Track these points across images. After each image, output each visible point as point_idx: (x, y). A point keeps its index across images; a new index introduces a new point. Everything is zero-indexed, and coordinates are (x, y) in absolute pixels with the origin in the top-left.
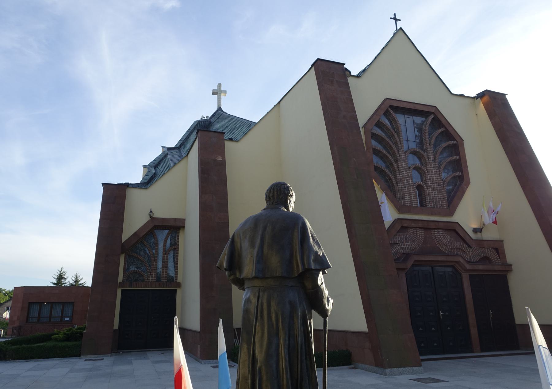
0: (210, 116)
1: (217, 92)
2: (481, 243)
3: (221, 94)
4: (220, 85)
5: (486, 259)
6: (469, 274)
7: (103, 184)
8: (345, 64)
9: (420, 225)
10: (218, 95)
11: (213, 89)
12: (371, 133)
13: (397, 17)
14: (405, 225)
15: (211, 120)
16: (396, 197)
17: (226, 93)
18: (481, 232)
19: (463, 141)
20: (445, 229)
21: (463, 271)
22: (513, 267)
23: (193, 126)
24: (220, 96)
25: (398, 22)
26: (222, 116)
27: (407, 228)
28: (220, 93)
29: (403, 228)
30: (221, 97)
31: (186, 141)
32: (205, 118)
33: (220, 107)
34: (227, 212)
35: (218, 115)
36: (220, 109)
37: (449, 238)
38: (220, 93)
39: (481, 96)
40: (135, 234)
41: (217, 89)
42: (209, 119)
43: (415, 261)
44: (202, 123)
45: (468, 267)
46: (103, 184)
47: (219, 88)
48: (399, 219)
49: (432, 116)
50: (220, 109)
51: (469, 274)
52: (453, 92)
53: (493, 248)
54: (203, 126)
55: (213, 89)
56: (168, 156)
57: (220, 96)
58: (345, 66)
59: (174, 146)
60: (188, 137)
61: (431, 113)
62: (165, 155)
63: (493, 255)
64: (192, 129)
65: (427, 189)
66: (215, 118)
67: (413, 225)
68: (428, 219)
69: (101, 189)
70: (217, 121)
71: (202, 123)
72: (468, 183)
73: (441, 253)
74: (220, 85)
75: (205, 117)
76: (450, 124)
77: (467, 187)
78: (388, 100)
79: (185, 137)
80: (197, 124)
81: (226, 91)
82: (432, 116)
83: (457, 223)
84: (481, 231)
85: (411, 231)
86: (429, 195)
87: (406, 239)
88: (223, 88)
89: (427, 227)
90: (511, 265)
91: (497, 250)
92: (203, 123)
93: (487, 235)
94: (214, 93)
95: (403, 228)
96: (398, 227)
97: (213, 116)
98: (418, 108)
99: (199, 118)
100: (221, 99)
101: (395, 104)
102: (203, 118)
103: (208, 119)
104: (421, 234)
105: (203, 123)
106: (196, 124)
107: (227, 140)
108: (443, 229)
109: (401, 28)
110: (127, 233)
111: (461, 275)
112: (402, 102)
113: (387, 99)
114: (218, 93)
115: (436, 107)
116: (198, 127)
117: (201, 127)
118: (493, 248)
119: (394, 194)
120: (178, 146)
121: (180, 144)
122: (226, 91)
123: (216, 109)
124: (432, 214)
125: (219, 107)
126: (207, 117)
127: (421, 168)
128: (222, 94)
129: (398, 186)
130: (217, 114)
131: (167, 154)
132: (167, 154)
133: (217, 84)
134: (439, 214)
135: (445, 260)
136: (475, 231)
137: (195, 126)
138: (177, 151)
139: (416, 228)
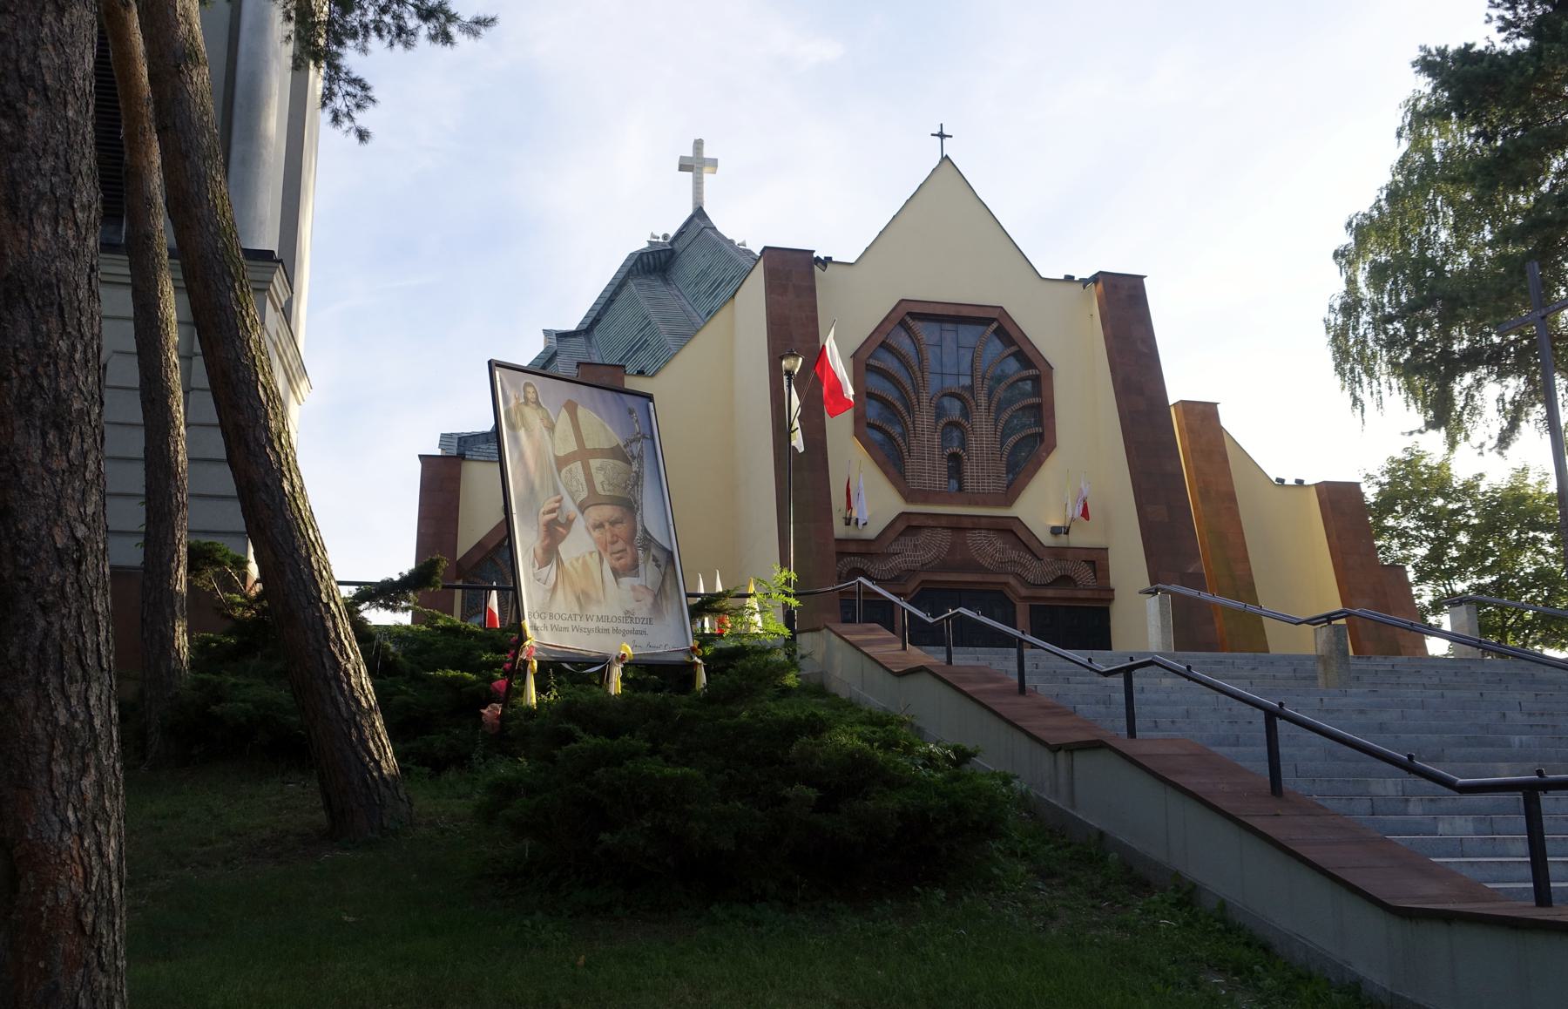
0: (672, 234)
1: (695, 164)
2: (1059, 553)
3: (701, 169)
4: (698, 144)
5: (1065, 580)
6: (1030, 605)
7: (420, 456)
8: (814, 251)
9: (944, 522)
10: (695, 171)
11: (681, 157)
12: (867, 365)
13: (945, 132)
14: (914, 523)
15: (676, 246)
16: (905, 479)
17: (716, 166)
18: (1067, 533)
19: (1052, 369)
20: (994, 530)
21: (1018, 600)
22: (1116, 593)
23: (625, 270)
24: (698, 176)
25: (946, 141)
26: (700, 238)
27: (919, 528)
28: (699, 166)
29: (909, 528)
30: (702, 178)
31: (605, 312)
32: (661, 240)
33: (701, 209)
34: (1230, 475)
35: (693, 232)
36: (699, 213)
37: (999, 544)
38: (699, 166)
39: (1100, 277)
40: (479, 545)
41: (691, 155)
42: (671, 243)
43: (923, 581)
44: (648, 258)
45: (1024, 592)
46: (420, 456)
47: (697, 153)
48: (903, 513)
49: (995, 325)
50: (699, 213)
51: (1030, 605)
52: (1043, 276)
53: (1085, 561)
54: (652, 267)
55: (681, 157)
56: (558, 359)
57: (698, 176)
58: (815, 255)
59: (573, 328)
60: (613, 301)
61: (994, 320)
62: (550, 355)
63: (1084, 575)
64: (621, 276)
65: (969, 459)
66: (686, 240)
67: (931, 522)
68: (914, 511)
69: (418, 465)
70: (689, 250)
71: (648, 258)
72: (1053, 446)
73: (979, 568)
74: (698, 144)
75: (661, 237)
76: (1028, 339)
77: (1049, 454)
78: (904, 302)
79: (603, 301)
80: (635, 264)
81: (716, 160)
82: (995, 325)
83: (1017, 518)
84: (1068, 531)
85: (926, 533)
86: (969, 470)
87: (915, 546)
88: (707, 153)
89: (958, 526)
90: (1113, 590)
91: (1092, 563)
92: (651, 257)
93: (1078, 539)
94: (682, 168)
95: (909, 528)
96: (901, 526)
97: (680, 233)
98: (965, 312)
99: (643, 244)
100: (703, 183)
101: (917, 310)
102: (655, 240)
103: (669, 240)
104: (944, 538)
105: (651, 257)
106: (633, 262)
107: (632, 375)
108: (989, 529)
109: (947, 156)
110: (464, 545)
111: (1014, 605)
112: (932, 305)
113: (903, 300)
114: (693, 166)
115: (1002, 308)
116: (637, 269)
117: (646, 268)
118: (1085, 561)
119: (902, 474)
120: (585, 326)
121: (590, 320)
122: (716, 160)
123: (689, 212)
124: (969, 504)
125: (697, 206)
126: (665, 237)
127: (960, 423)
128: (706, 169)
129: (910, 456)
130: (691, 227)
131: (555, 354)
132: (555, 354)
133: (693, 141)
134: (985, 504)
135: (981, 580)
136: (1055, 531)
137: (631, 269)
138: (582, 339)
139: (936, 527)
